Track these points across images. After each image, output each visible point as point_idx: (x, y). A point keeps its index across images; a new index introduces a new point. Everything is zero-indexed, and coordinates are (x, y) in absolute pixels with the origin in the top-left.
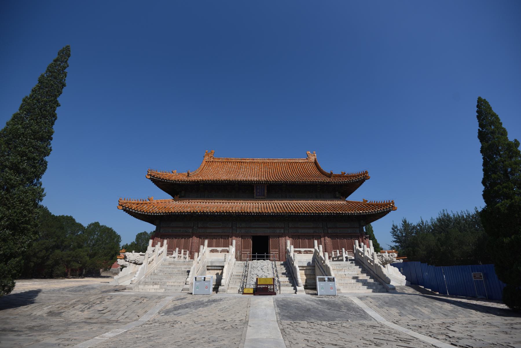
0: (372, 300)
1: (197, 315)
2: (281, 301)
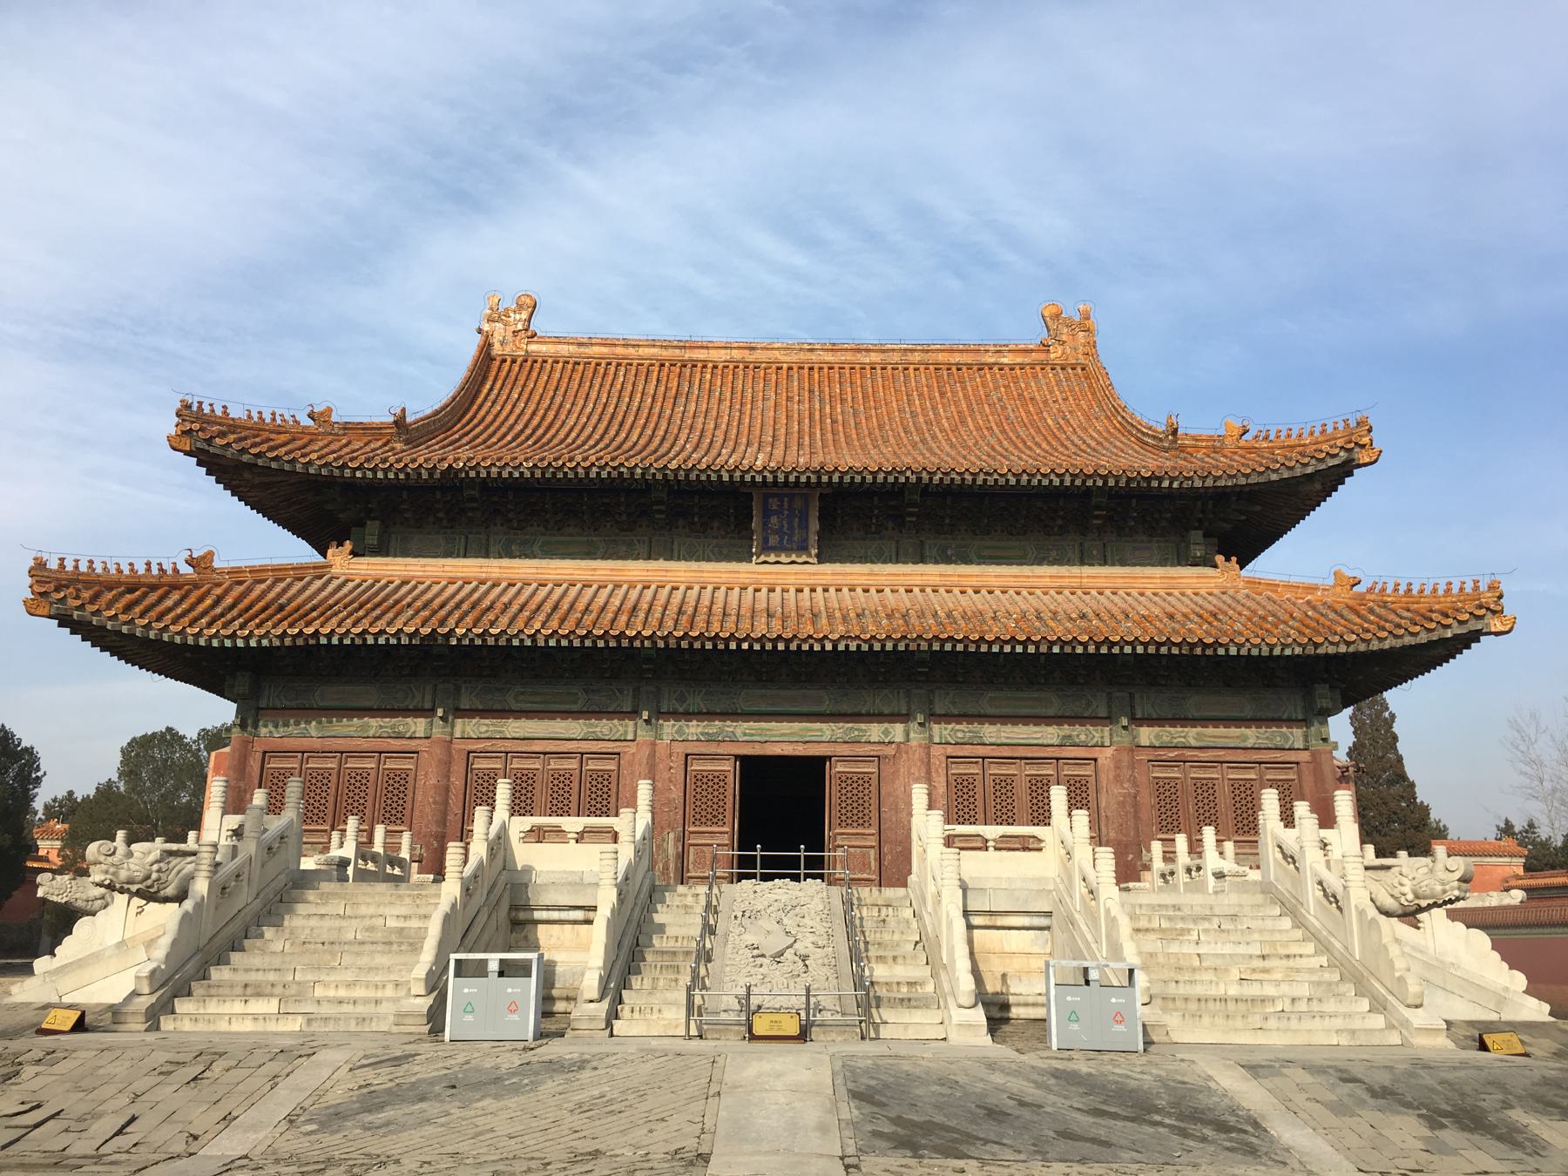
0: (1307, 1078)
1: (471, 1132)
2: (866, 1071)
